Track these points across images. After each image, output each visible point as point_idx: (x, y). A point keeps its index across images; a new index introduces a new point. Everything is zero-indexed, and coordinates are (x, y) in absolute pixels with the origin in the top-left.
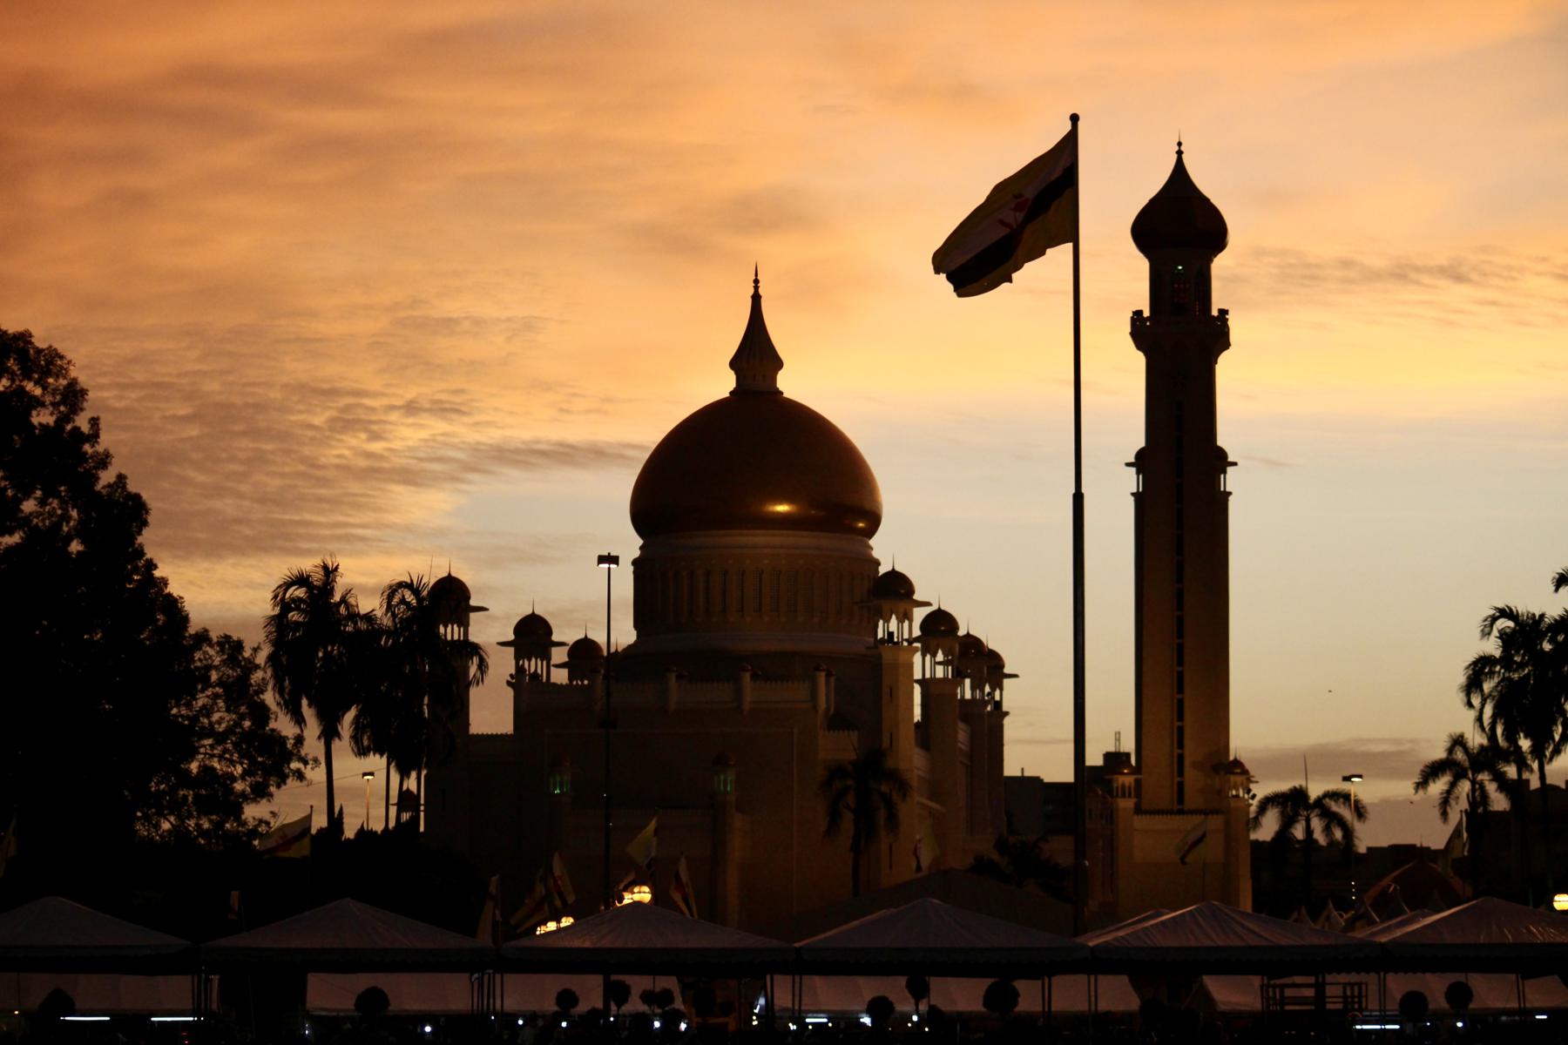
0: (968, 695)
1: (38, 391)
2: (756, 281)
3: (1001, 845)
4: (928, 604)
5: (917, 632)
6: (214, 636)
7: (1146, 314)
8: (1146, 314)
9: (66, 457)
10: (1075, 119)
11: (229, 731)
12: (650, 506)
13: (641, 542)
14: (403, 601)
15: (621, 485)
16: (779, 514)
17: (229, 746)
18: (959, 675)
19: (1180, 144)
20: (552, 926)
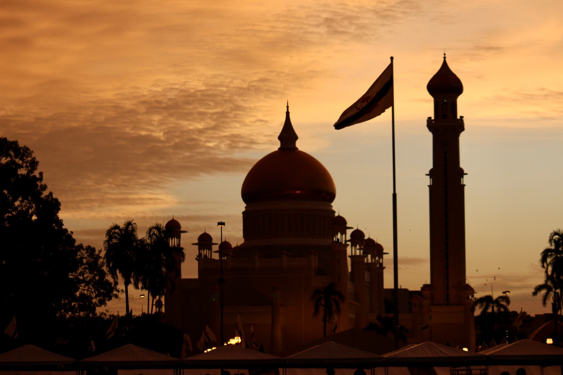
0: (370, 261)
1: (20, 162)
2: (288, 107)
3: (379, 318)
4: (352, 228)
5: (348, 238)
6: (85, 246)
7: (433, 118)
8: (433, 118)
9: (31, 186)
10: (392, 58)
11: (91, 280)
12: (248, 193)
13: (245, 205)
14: (154, 234)
15: (239, 178)
16: (298, 194)
17: (91, 286)
18: (366, 254)
19: (445, 54)
20: (209, 350)
